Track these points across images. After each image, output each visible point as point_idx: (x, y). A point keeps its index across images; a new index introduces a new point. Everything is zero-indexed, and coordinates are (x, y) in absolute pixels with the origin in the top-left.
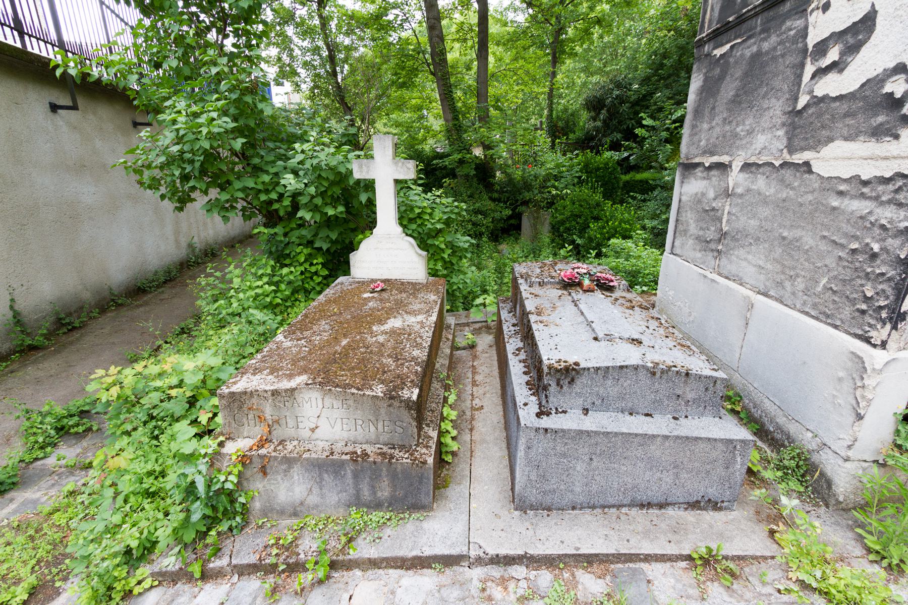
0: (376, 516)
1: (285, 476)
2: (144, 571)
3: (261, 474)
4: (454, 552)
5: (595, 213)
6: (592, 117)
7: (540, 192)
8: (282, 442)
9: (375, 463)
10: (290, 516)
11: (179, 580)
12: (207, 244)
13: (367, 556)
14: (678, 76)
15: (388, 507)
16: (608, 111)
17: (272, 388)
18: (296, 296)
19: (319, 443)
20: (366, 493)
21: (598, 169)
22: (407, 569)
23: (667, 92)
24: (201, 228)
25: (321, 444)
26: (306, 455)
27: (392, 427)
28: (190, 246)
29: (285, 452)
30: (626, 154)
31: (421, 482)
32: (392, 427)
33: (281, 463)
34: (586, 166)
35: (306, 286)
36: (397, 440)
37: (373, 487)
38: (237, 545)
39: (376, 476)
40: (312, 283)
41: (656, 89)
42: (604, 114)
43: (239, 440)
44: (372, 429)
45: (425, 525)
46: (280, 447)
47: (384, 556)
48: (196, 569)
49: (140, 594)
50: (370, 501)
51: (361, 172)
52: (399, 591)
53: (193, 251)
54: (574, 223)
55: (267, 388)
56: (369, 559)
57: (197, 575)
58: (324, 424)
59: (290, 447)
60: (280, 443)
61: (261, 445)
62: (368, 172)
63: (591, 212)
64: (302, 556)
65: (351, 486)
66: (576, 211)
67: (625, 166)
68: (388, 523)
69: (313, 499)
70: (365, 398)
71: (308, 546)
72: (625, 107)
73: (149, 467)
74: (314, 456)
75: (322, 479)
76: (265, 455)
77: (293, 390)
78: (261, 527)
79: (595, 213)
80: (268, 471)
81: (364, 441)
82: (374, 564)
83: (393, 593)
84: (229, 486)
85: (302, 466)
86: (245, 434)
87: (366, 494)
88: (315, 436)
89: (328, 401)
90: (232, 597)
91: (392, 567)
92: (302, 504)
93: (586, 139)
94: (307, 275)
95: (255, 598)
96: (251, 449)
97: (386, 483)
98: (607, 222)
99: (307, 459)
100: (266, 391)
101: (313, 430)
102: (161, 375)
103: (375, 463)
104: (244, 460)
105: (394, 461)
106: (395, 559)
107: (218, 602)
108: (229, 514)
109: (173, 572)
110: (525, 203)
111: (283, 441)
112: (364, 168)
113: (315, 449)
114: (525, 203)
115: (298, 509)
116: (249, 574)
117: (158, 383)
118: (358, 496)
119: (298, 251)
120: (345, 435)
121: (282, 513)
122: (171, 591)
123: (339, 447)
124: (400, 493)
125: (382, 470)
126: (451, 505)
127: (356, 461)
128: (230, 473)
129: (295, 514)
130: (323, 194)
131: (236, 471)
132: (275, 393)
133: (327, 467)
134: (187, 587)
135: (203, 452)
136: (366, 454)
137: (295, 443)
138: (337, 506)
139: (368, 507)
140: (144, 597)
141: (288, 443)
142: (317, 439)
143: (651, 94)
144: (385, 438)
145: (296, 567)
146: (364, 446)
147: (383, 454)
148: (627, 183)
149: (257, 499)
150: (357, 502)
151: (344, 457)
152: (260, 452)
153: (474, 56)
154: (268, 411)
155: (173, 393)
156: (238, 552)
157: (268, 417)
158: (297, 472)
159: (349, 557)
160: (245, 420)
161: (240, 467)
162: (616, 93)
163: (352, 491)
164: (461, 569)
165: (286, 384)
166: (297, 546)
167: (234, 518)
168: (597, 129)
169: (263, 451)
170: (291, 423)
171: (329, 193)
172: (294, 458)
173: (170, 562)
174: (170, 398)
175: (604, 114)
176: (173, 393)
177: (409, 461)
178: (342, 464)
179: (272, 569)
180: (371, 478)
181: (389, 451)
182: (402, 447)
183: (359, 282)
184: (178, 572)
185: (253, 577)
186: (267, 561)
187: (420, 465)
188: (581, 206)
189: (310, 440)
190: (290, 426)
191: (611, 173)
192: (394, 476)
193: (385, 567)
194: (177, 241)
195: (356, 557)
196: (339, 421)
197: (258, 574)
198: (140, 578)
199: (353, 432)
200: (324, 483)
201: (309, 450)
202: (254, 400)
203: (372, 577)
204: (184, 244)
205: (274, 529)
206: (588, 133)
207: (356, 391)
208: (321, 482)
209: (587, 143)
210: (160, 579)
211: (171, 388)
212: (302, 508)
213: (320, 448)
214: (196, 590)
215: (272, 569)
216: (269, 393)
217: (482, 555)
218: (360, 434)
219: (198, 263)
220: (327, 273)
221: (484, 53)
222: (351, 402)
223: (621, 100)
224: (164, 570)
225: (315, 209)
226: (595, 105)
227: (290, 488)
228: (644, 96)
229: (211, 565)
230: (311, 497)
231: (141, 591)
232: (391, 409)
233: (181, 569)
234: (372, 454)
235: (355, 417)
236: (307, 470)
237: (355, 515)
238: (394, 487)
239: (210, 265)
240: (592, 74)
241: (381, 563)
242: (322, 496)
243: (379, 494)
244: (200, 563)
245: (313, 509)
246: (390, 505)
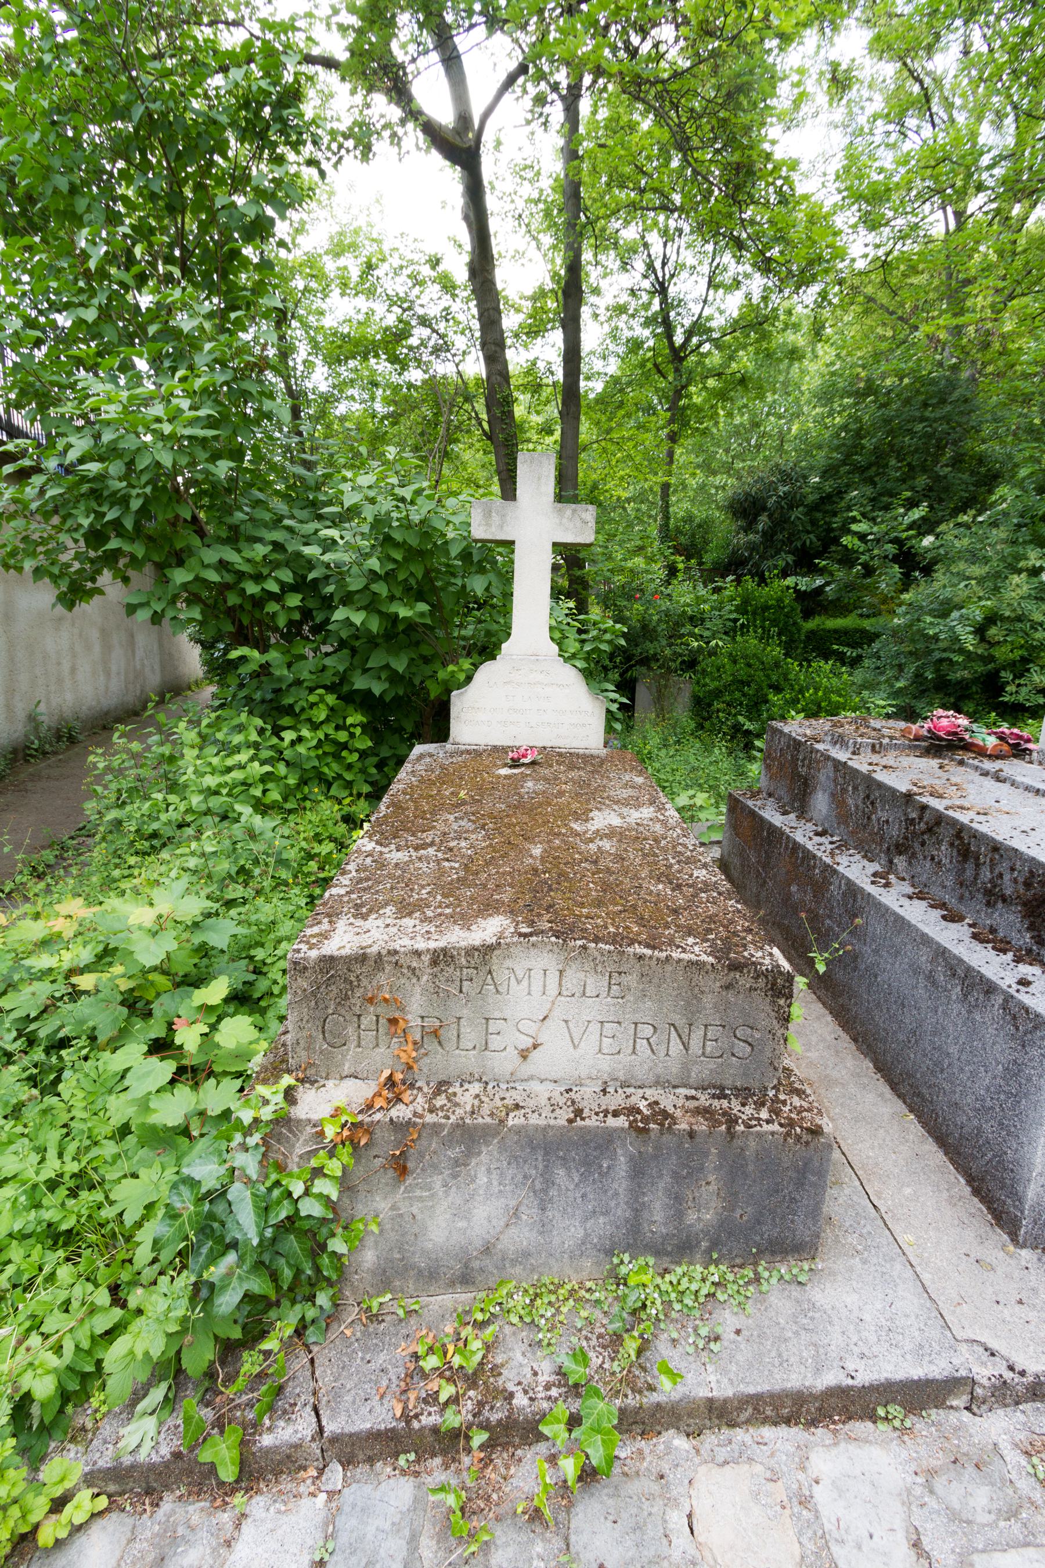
0: (694, 1275)
1: (455, 1176)
2: (65, 1466)
3: (391, 1173)
4: (936, 1369)
5: (774, 678)
6: (741, 527)
7: (670, 645)
8: (441, 1087)
9: (692, 1134)
10: (452, 1284)
11: (167, 1487)
12: (62, 718)
13: (703, 1393)
14: (886, 466)
15: (709, 1251)
16: (770, 517)
17: (432, 945)
18: (306, 790)
19: (535, 1086)
20: (658, 1216)
21: (766, 608)
22: (813, 1423)
23: (869, 491)
24: (53, 688)
25: (542, 1091)
26: (514, 1120)
27: (724, 1043)
28: (32, 718)
29: (459, 1111)
30: (819, 582)
31: (800, 1184)
32: (724, 1043)
33: (448, 1142)
34: (746, 602)
35: (326, 770)
36: (732, 1078)
37: (678, 1199)
38: (326, 1375)
39: (689, 1173)
40: (335, 766)
41: (848, 485)
42: (763, 522)
43: (330, 1083)
44: (676, 1047)
45: (822, 1295)
46: (440, 1101)
47: (751, 1390)
48: (222, 1454)
49: (59, 1543)
50: (665, 1237)
51: (488, 525)
52: (821, 1495)
53: (36, 729)
54: (737, 695)
55: (421, 945)
56: (710, 1401)
57: (228, 1473)
58: (554, 1037)
59: (467, 1096)
60: (437, 1093)
61: (393, 1089)
62: (501, 527)
63: (768, 676)
64: (520, 1400)
65: (623, 1198)
66: (742, 675)
67: (811, 603)
68: (721, 1296)
69: (520, 1237)
70: (669, 968)
71: (525, 1371)
72: (798, 513)
73: (52, 1167)
74: (534, 1120)
75: (549, 1182)
76: (409, 1122)
77: (487, 950)
78: (375, 1318)
79: (774, 678)
80: (410, 1165)
81: (652, 1078)
82: (721, 1414)
83: (805, 1501)
84: (311, 1208)
85: (502, 1148)
86: (347, 1069)
87: (657, 1217)
88: (527, 1069)
89: (574, 977)
90: (343, 1538)
91: (766, 1421)
92: (487, 1250)
93: (730, 564)
94: (328, 748)
95: (413, 1540)
96: (370, 1106)
97: (713, 1188)
98: (801, 691)
99: (518, 1130)
100: (418, 953)
101: (524, 1054)
102: (45, 944)
103: (692, 1134)
104: (357, 1136)
105: (741, 1128)
106: (776, 1399)
107: (306, 1560)
108: (301, 1289)
109: (152, 1467)
110: (645, 661)
111: (441, 1083)
112: (495, 518)
113: (531, 1103)
114: (645, 661)
115: (476, 1265)
116: (371, 1460)
117: (44, 961)
118: (634, 1226)
119: (313, 698)
120: (605, 1065)
121: (430, 1276)
122: (150, 1525)
123: (587, 1095)
124: (744, 1213)
125: (706, 1154)
126: (852, 1239)
127: (645, 1131)
128: (318, 1172)
129: (465, 1279)
130: (388, 577)
131: (334, 1167)
132: (441, 958)
133: (566, 1149)
134: (195, 1511)
135: (246, 1116)
136: (665, 1114)
137: (476, 1088)
138: (576, 1254)
139: (658, 1253)
140: (71, 1552)
141: (456, 1088)
142: (531, 1078)
143: (840, 493)
144: (702, 1071)
145: (517, 1433)
146: (653, 1094)
147: (705, 1112)
148: (812, 634)
149: (370, 1241)
150: (634, 1240)
151: (612, 1122)
152: (394, 1113)
153: (556, 414)
154: (416, 1005)
155: (85, 982)
156: (336, 1394)
157: (415, 1022)
158: (486, 1168)
159: (655, 1398)
160: (350, 1030)
161: (345, 1153)
162: (783, 489)
163: (622, 1211)
164: (953, 1417)
165: (457, 937)
166: (496, 1371)
167: (311, 1298)
168: (752, 547)
169: (400, 1112)
170: (470, 1035)
171: (401, 577)
172: (487, 1126)
173: (143, 1437)
174: (75, 994)
175: (763, 522)
176: (85, 982)
177: (775, 1127)
178: (606, 1141)
179: (449, 1443)
180: (676, 1176)
181: (716, 1103)
182: (744, 1094)
183: (468, 752)
184: (166, 1464)
185: (383, 1468)
186: (425, 1420)
187: (805, 1137)
188: (749, 665)
189: (512, 1080)
190: (466, 1043)
191: (787, 616)
192: (734, 1169)
193: (747, 1422)
194: (9, 707)
195: (676, 1396)
196: (595, 1027)
197: (402, 1461)
198: (58, 1492)
199: (626, 1058)
200: (553, 1192)
201: (517, 1107)
202: (382, 978)
203: (722, 1454)
204: (21, 714)
205: (413, 1321)
206: (734, 552)
207: (648, 952)
208: (545, 1191)
209: (733, 565)
210: (112, 1488)
211: (81, 971)
212: (487, 1262)
213: (543, 1101)
214: (225, 1517)
215: (449, 1443)
216: (426, 958)
217: (1008, 1375)
218: (641, 1062)
219: (45, 753)
220: (370, 744)
221: (573, 409)
222: (631, 980)
223: (792, 501)
224: (127, 1460)
225: (372, 606)
226: (746, 509)
227: (464, 1210)
228: (829, 496)
229: (267, 1440)
230: (513, 1231)
231: (63, 1534)
232: (731, 996)
233: (177, 1455)
234: (678, 1113)
235: (637, 1017)
236: (513, 1159)
237: (641, 1273)
238: (731, 1198)
239: (121, 727)
240: (714, 473)
241: (740, 1409)
242: (544, 1227)
243: (691, 1217)
244: (234, 1434)
245: (514, 1262)
246: (714, 1245)
